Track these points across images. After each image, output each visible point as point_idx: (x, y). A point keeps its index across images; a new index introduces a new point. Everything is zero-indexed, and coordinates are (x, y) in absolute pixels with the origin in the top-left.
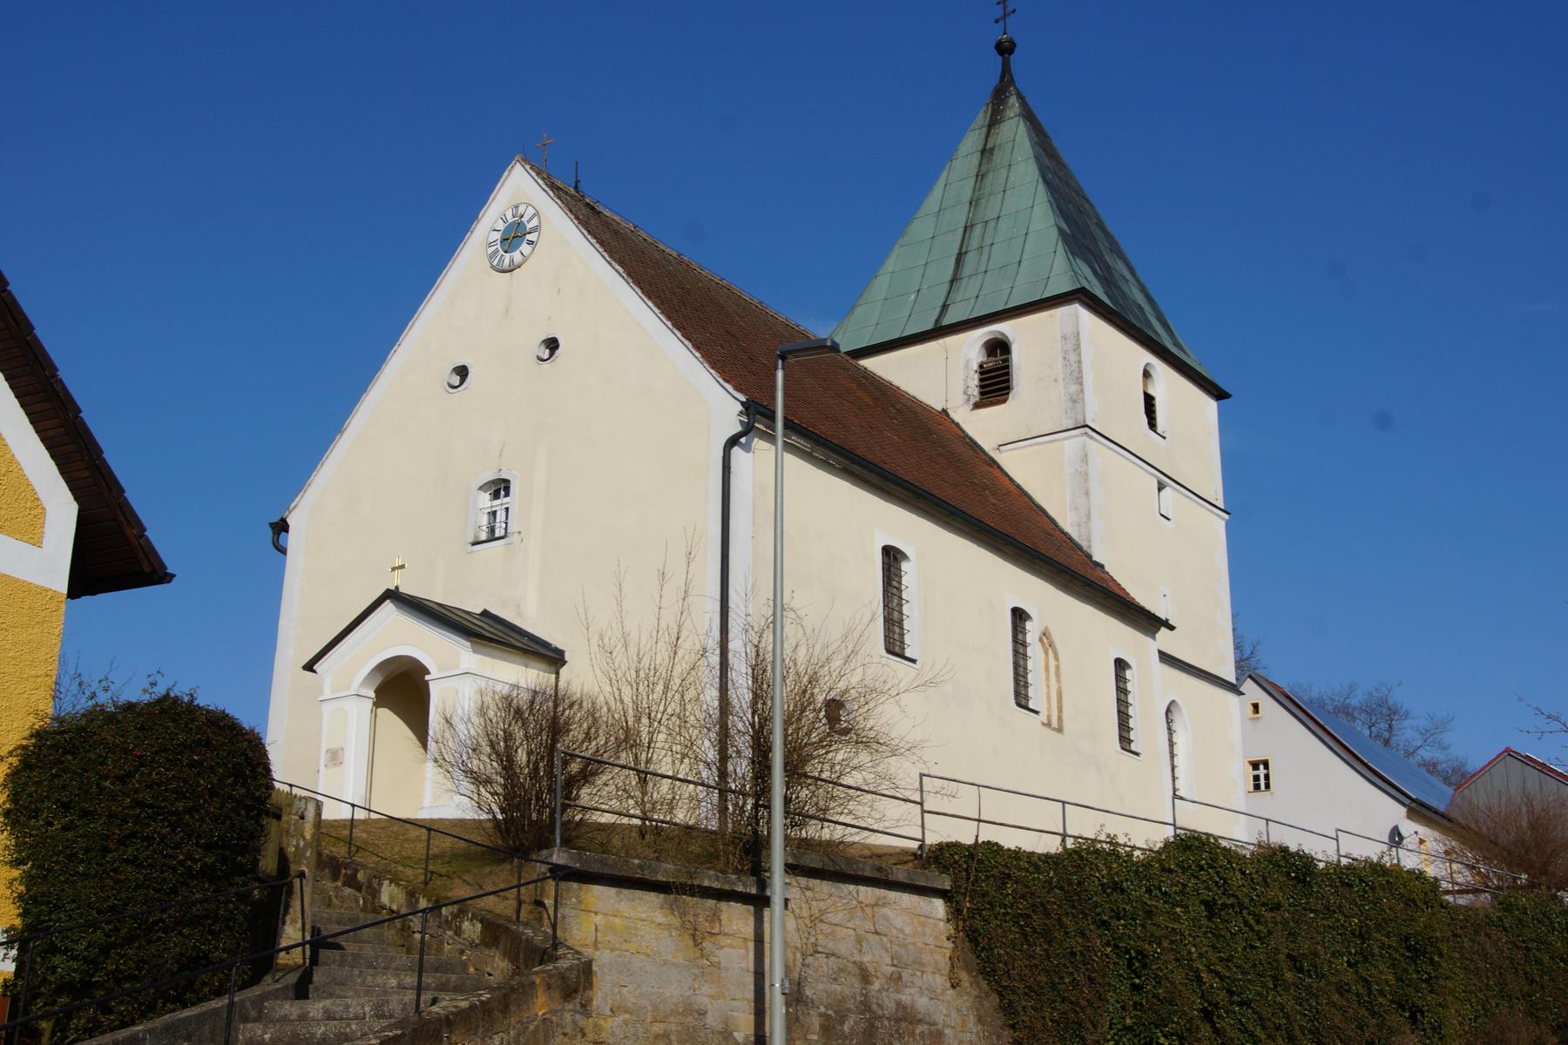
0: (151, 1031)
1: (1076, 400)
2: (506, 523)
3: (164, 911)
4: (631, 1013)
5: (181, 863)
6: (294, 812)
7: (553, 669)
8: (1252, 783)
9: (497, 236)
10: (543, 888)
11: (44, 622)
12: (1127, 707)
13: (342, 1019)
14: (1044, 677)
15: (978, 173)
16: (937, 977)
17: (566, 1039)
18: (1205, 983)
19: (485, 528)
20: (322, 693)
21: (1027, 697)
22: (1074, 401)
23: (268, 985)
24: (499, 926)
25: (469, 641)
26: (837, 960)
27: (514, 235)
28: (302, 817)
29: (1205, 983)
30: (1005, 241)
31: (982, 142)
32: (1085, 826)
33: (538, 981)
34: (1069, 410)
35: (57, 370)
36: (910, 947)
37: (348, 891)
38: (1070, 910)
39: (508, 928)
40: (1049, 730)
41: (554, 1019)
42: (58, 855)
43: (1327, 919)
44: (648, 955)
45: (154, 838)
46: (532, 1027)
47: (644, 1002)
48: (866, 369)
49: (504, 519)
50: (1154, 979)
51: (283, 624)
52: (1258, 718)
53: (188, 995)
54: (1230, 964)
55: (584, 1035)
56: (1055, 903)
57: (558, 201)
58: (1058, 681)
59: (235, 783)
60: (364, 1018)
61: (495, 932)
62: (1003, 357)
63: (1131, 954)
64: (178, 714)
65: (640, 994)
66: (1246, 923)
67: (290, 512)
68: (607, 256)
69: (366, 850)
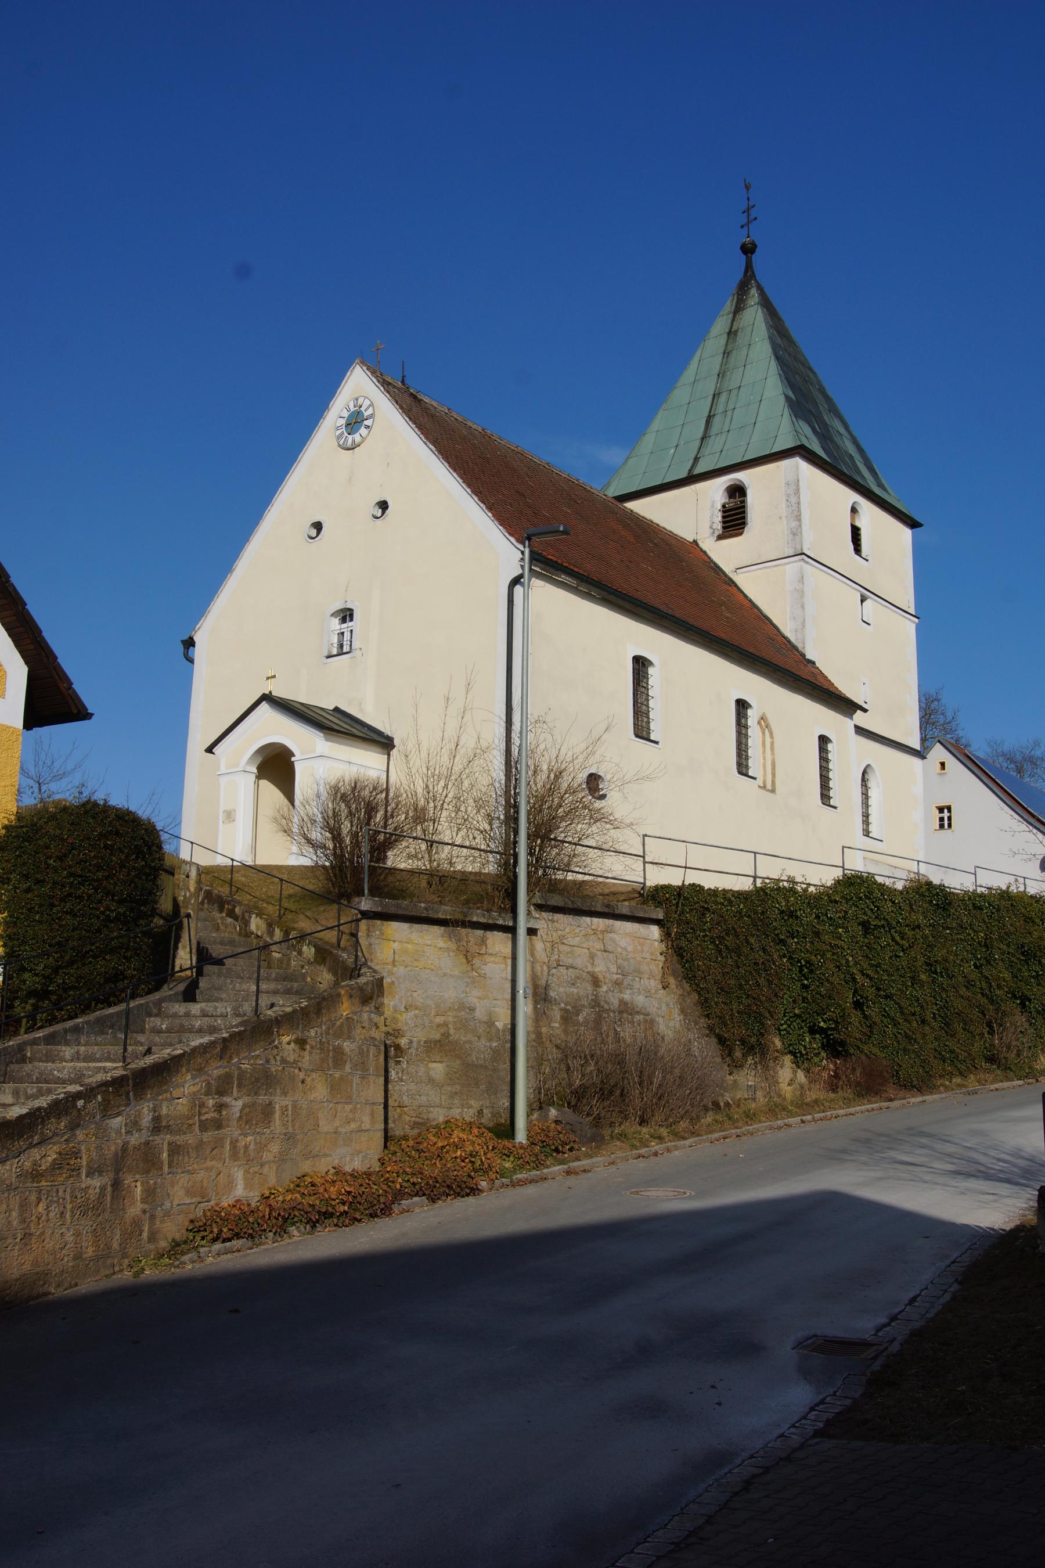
0: (87, 1023)
1: (796, 533)
2: (351, 642)
3: (93, 944)
4: (420, 1010)
5: (102, 913)
6: (182, 872)
7: (385, 751)
8: (938, 823)
9: (343, 422)
10: (358, 926)
11: (8, 749)
12: (828, 772)
13: (212, 1016)
14: (761, 751)
15: (725, 351)
16: (652, 982)
17: (364, 1031)
18: (858, 983)
19: (336, 645)
20: (219, 769)
21: (747, 767)
22: (794, 534)
23: (165, 991)
24: (326, 950)
25: (322, 732)
26: (574, 970)
27: (355, 421)
28: (188, 877)
29: (858, 983)
30: (745, 406)
31: (729, 325)
32: (771, 870)
33: (343, 992)
34: (790, 541)
35: (10, 577)
36: (631, 961)
37: (229, 920)
38: (754, 932)
39: (331, 952)
40: (764, 791)
41: (355, 1018)
42: (23, 908)
43: (960, 934)
44: (432, 970)
45: (84, 897)
46: (338, 1023)
47: (429, 1002)
48: (632, 511)
49: (349, 638)
50: (818, 981)
51: (192, 715)
52: (945, 773)
53: (112, 999)
54: (878, 969)
55: (377, 1028)
56: (744, 928)
57: (387, 394)
58: (773, 753)
59: (137, 858)
60: (226, 1016)
61: (323, 955)
62: (741, 499)
63: (801, 963)
64: (97, 814)
65: (426, 997)
66: (893, 939)
67: (196, 632)
68: (423, 438)
69: (243, 890)
